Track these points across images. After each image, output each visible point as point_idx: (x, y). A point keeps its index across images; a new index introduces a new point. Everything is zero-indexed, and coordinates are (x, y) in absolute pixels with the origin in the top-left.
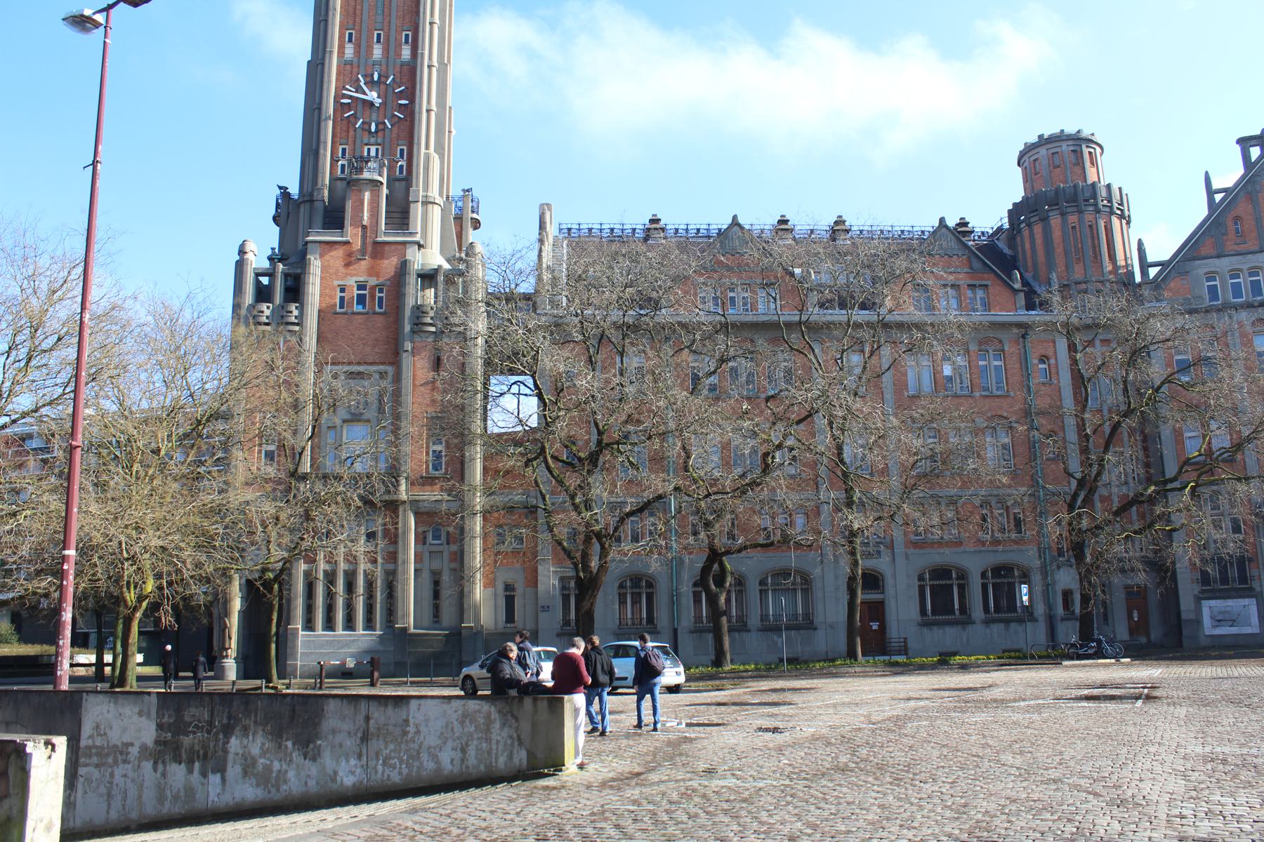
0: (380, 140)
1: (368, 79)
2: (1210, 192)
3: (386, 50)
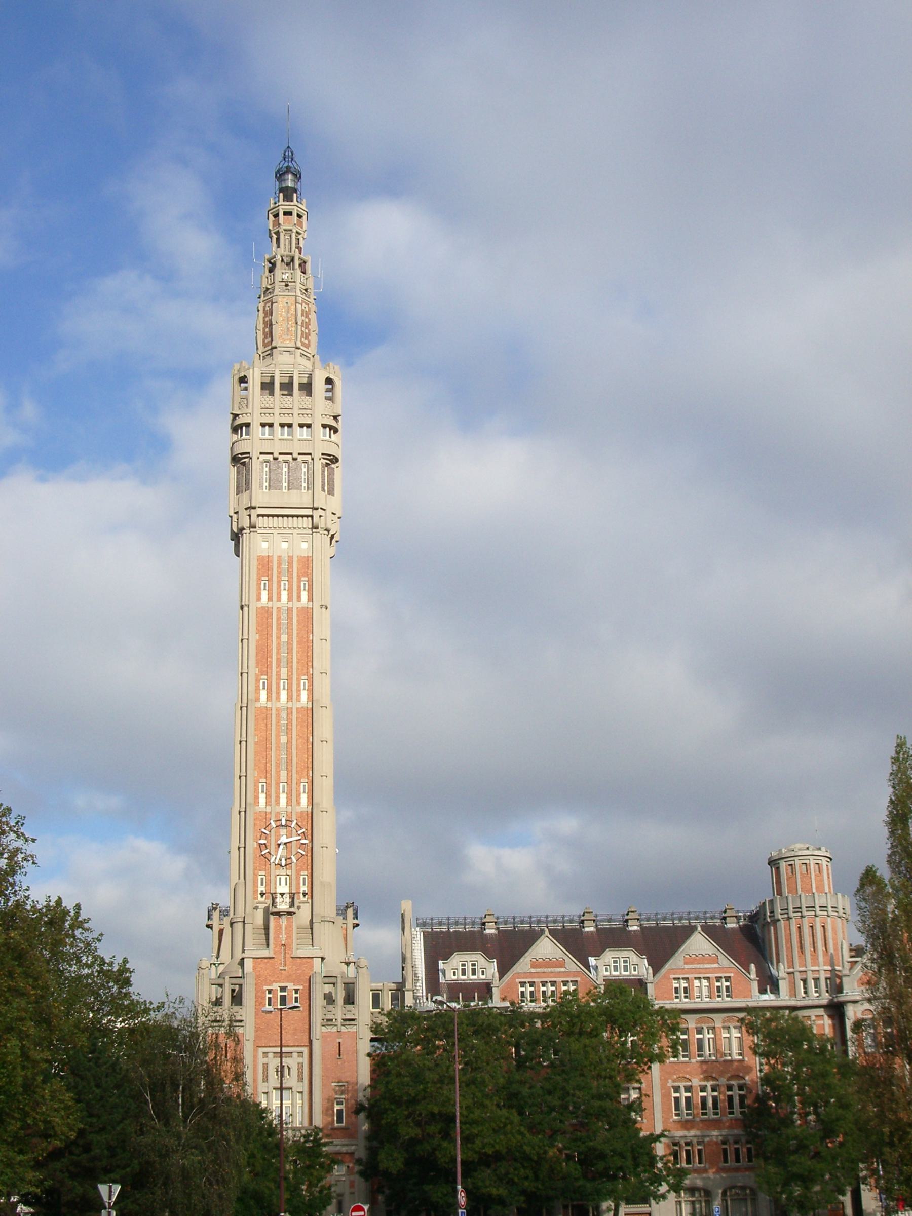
0: (289, 872)
1: (278, 823)
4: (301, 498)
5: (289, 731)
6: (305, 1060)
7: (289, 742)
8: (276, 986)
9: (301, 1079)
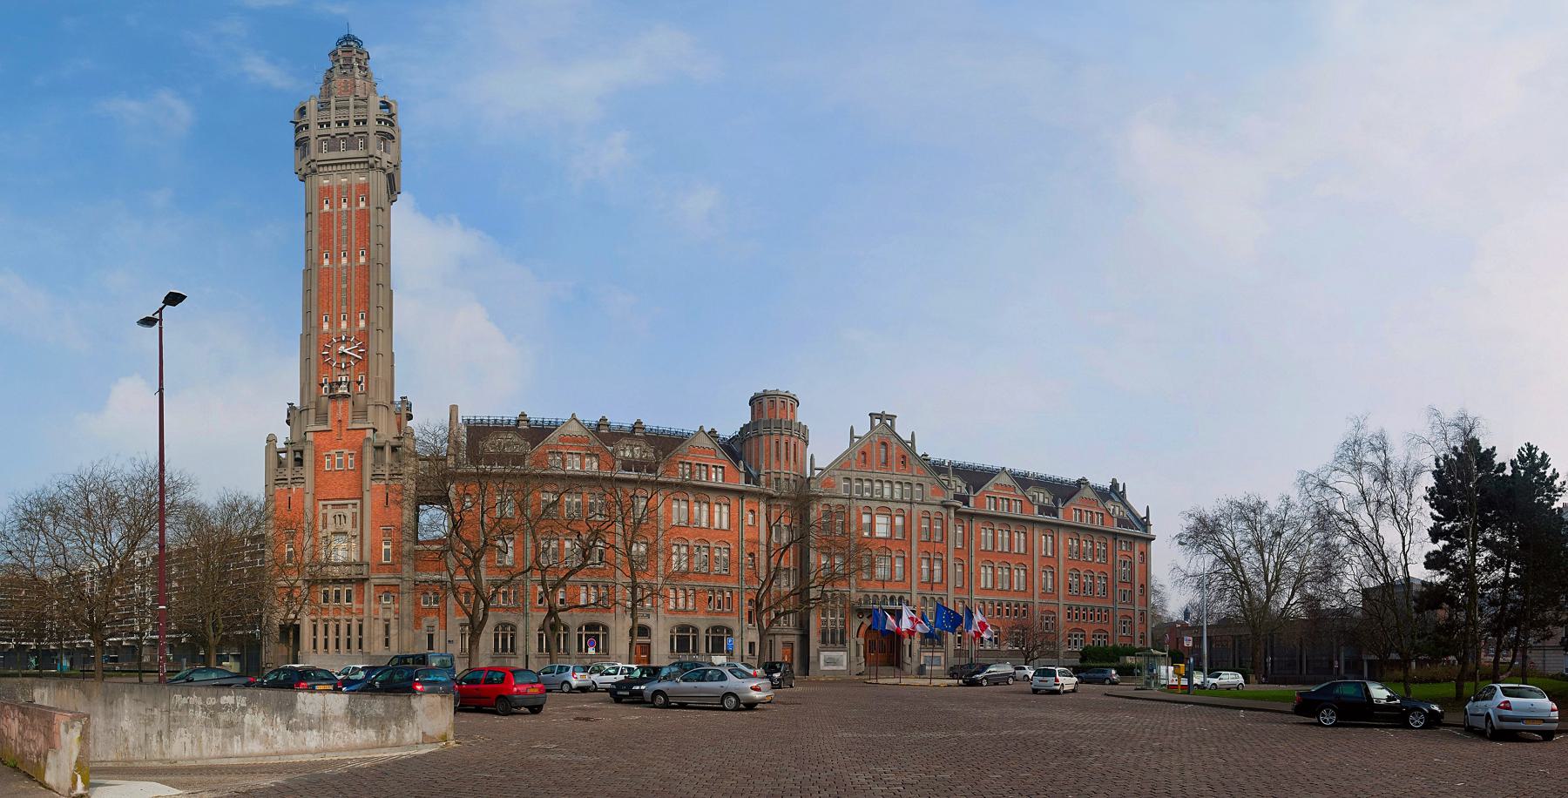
2: (852, 437)
3: (349, 324)
4: (361, 153)
5: (348, 280)
6: (357, 510)
7: (349, 287)
8: (333, 452)
9: (354, 526)
